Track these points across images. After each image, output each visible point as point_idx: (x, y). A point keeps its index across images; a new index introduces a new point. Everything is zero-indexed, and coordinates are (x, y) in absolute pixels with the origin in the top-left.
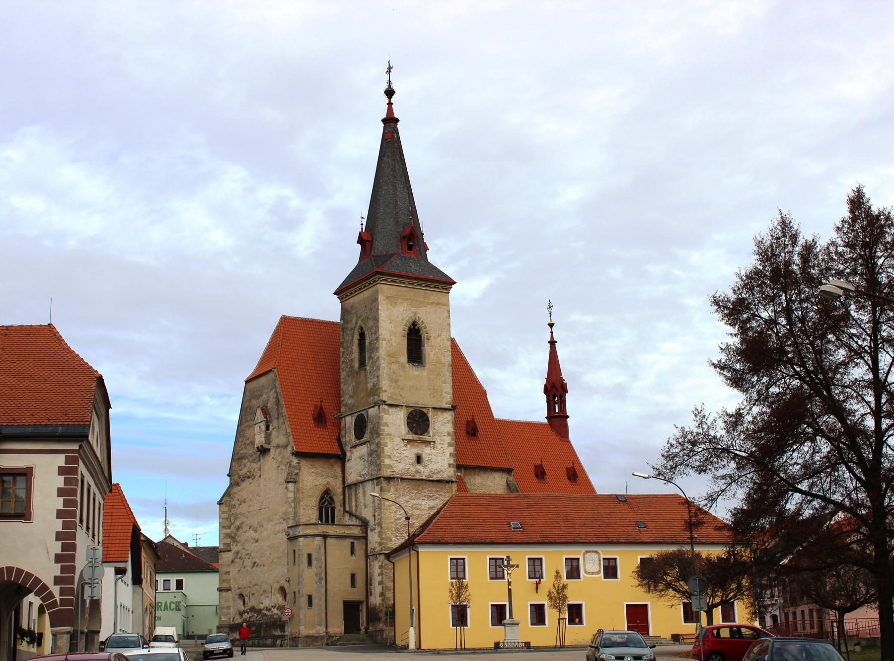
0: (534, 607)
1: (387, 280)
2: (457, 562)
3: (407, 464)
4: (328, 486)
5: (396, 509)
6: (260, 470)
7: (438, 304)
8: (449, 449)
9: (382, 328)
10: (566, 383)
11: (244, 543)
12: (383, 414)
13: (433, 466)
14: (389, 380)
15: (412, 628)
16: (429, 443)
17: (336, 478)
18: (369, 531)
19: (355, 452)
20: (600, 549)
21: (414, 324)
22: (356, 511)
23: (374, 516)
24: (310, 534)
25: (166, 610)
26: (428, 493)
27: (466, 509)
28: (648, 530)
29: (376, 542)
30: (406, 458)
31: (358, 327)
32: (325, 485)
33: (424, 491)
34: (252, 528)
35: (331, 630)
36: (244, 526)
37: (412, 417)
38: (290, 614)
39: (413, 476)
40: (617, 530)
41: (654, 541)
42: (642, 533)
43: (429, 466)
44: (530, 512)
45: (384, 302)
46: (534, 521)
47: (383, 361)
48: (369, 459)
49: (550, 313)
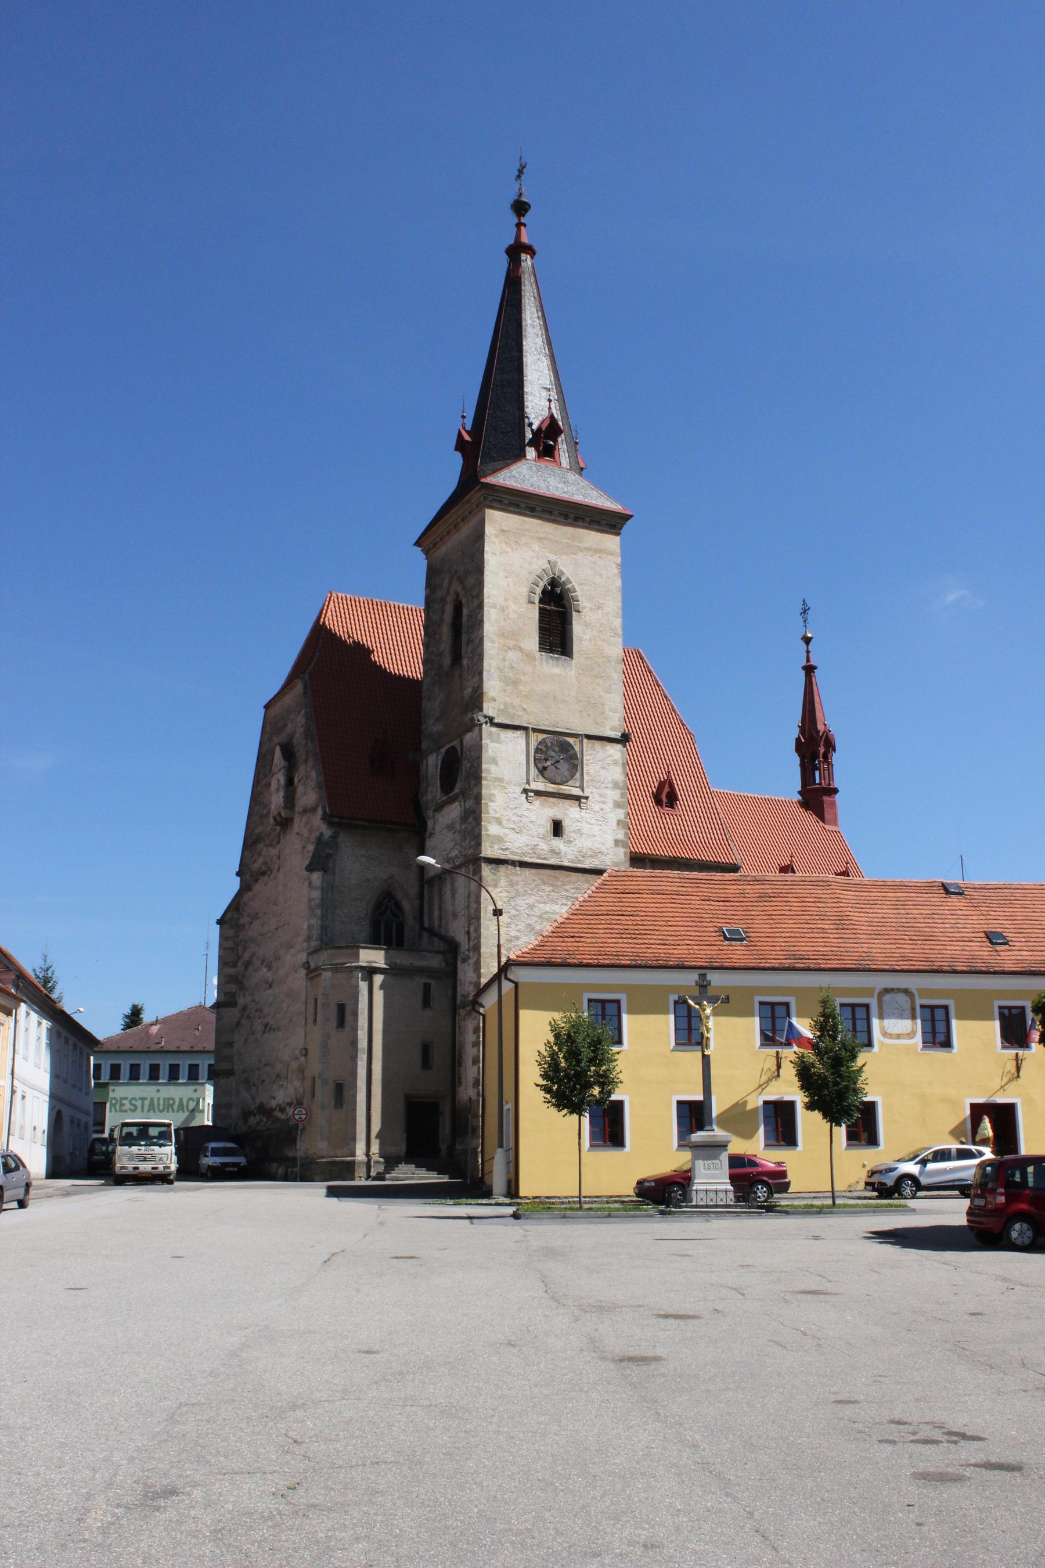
2: (603, 1009)
3: (533, 836)
5: (509, 920)
6: (279, 858)
7: (598, 551)
9: (490, 586)
12: (488, 741)
13: (583, 843)
14: (500, 680)
15: (499, 1151)
18: (459, 962)
19: (440, 819)
21: (554, 582)
22: (440, 926)
23: (468, 933)
25: (152, 1111)
26: (574, 893)
27: (628, 900)
28: (1013, 948)
29: (470, 983)
30: (531, 825)
33: (567, 887)
34: (265, 963)
36: (254, 959)
38: (304, 1117)
39: (545, 859)
40: (948, 947)
41: (1028, 969)
42: (1001, 953)
43: (576, 842)
44: (764, 908)
45: (494, 539)
46: (774, 926)
47: (490, 644)
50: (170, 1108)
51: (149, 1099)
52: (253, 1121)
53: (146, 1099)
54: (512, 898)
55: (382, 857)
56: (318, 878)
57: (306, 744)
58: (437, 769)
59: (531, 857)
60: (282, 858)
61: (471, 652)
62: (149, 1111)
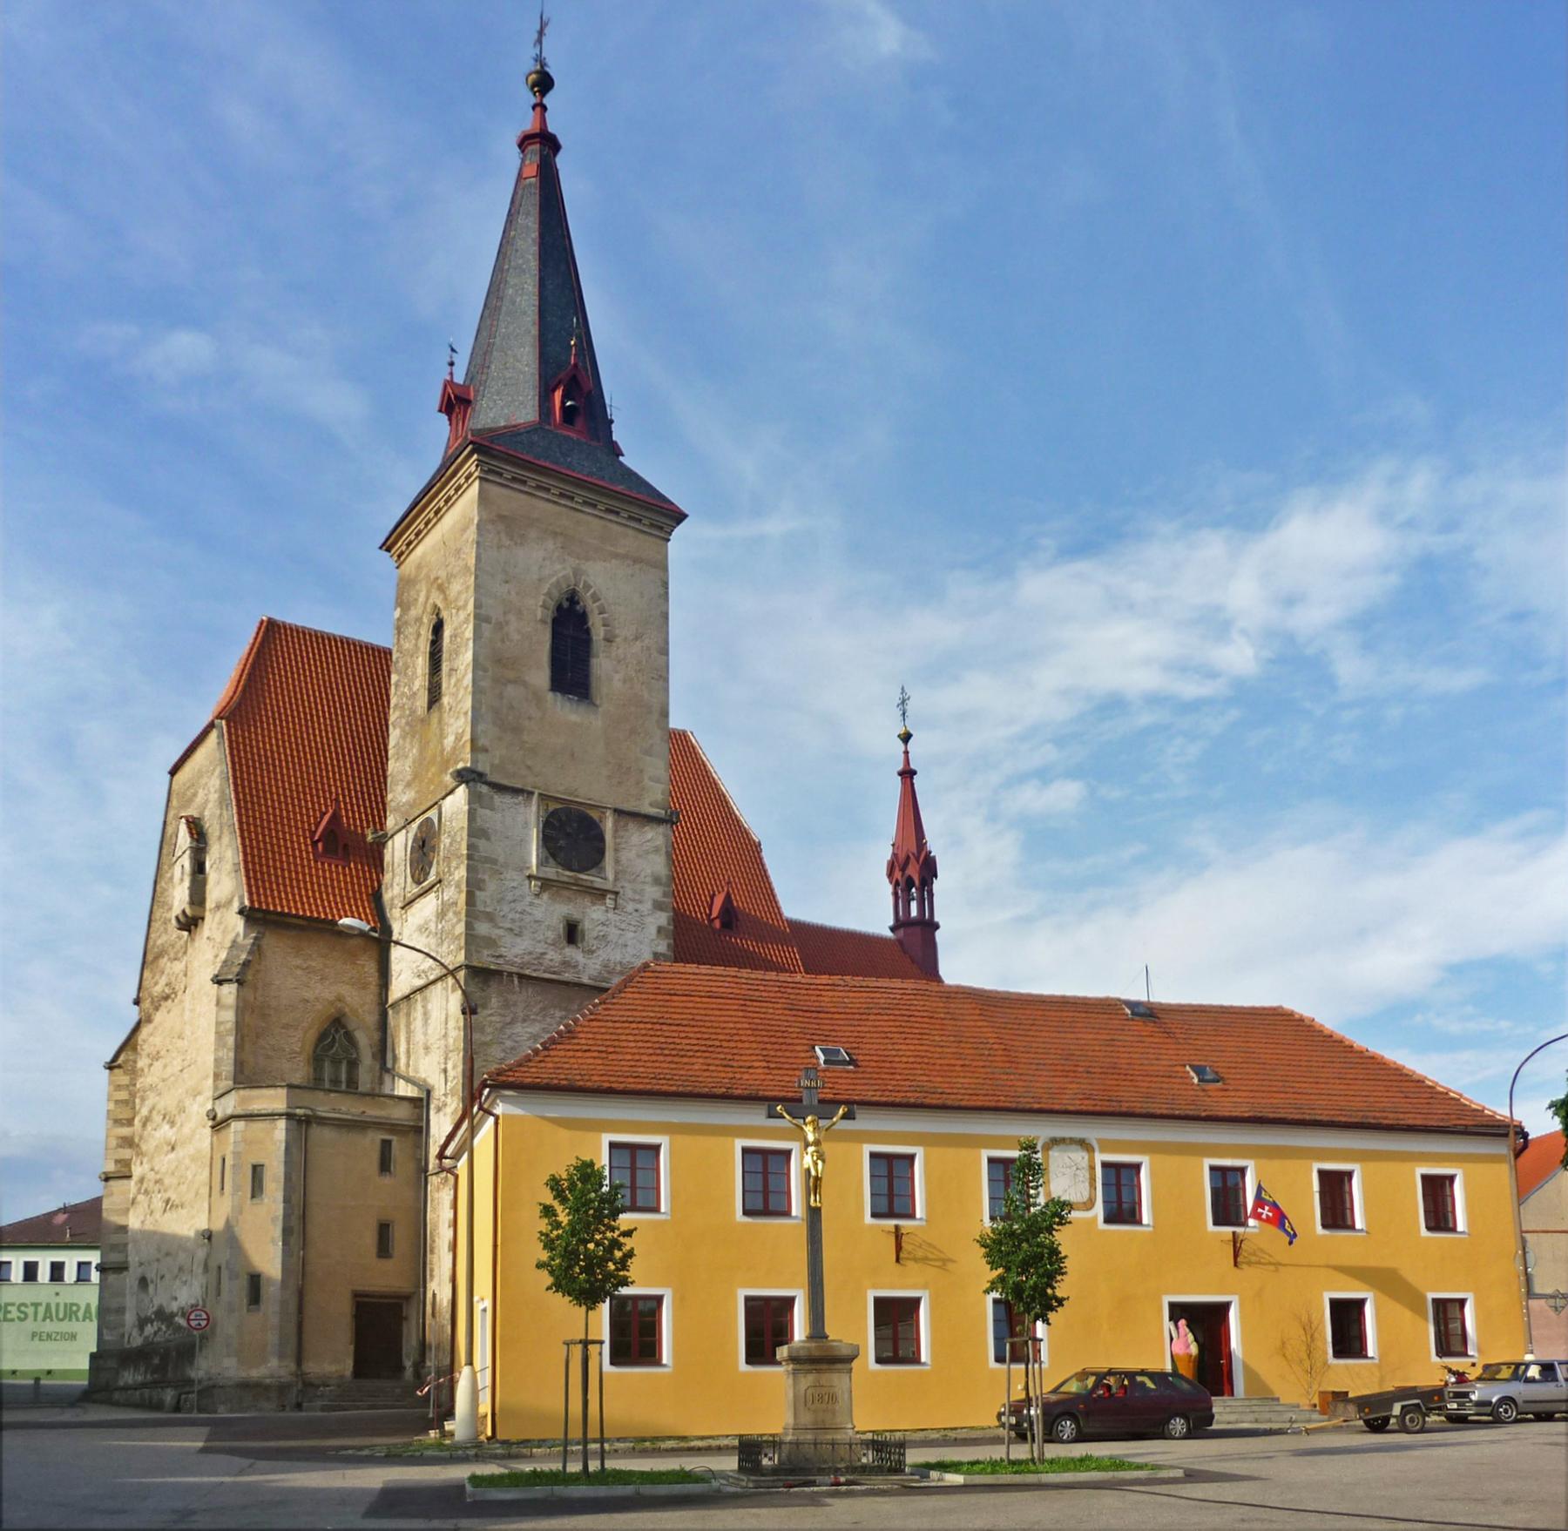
0: (1219, 1173)
1: (500, 475)
3: (539, 942)
4: (339, 1005)
6: (186, 975)
8: (657, 916)
10: (934, 857)
11: (152, 1157)
16: (600, 894)
17: (364, 987)
18: (432, 1112)
20: (1093, 1132)
21: (573, 597)
22: (408, 1065)
23: (445, 1071)
24: (263, 1112)
25: (48, 1320)
31: (429, 609)
32: (332, 1003)
34: (167, 1118)
35: (314, 1368)
37: (557, 824)
38: (203, 1323)
39: (554, 973)
43: (600, 952)
48: (440, 926)
49: (904, 714)
50: (73, 1317)
51: (44, 1305)
52: (149, 1330)
53: (40, 1304)
54: (508, 1024)
55: (327, 970)
56: (230, 993)
57: (221, 815)
58: (406, 851)
59: (535, 970)
60: (189, 973)
61: (455, 685)
62: (44, 1320)
